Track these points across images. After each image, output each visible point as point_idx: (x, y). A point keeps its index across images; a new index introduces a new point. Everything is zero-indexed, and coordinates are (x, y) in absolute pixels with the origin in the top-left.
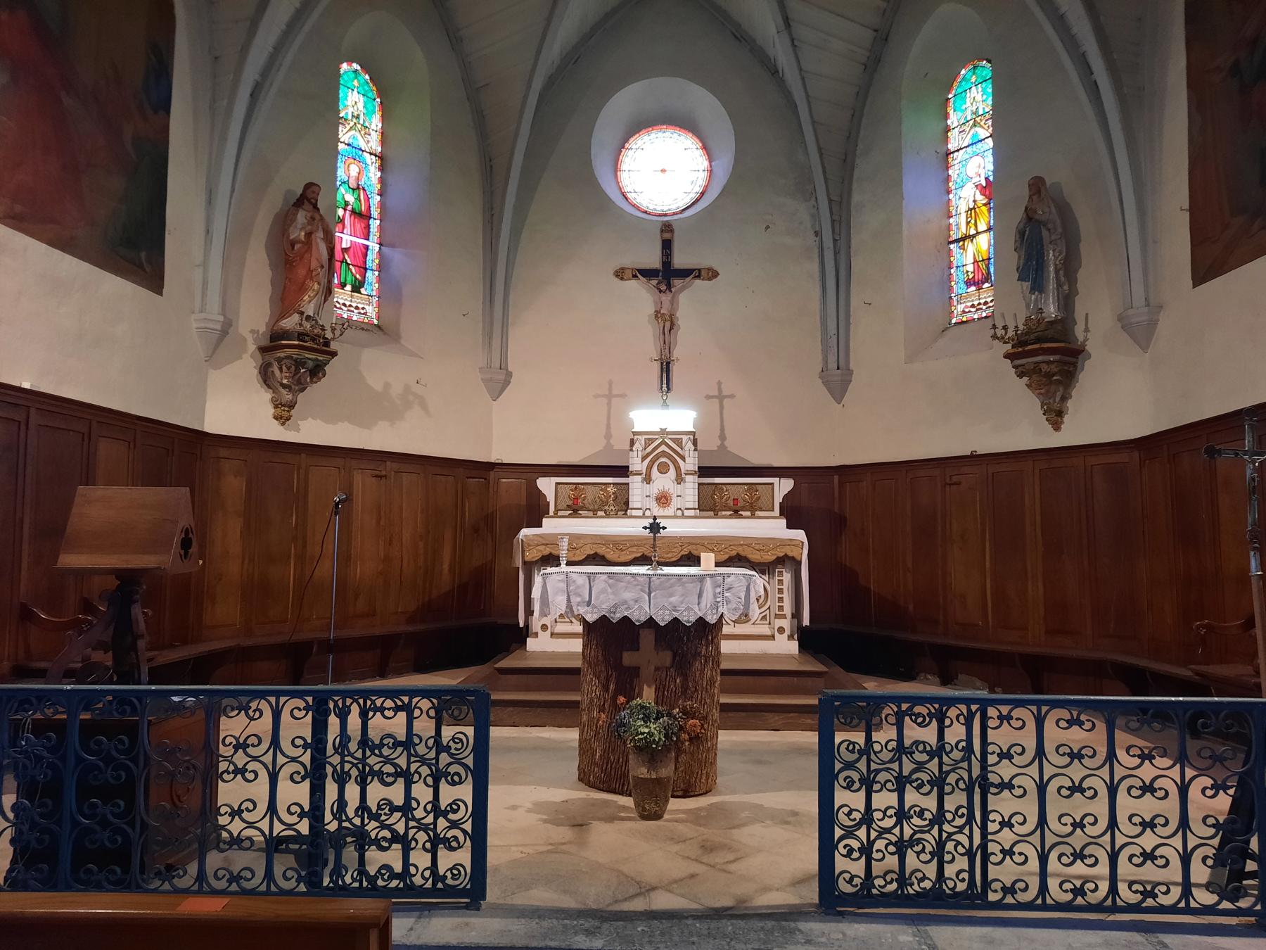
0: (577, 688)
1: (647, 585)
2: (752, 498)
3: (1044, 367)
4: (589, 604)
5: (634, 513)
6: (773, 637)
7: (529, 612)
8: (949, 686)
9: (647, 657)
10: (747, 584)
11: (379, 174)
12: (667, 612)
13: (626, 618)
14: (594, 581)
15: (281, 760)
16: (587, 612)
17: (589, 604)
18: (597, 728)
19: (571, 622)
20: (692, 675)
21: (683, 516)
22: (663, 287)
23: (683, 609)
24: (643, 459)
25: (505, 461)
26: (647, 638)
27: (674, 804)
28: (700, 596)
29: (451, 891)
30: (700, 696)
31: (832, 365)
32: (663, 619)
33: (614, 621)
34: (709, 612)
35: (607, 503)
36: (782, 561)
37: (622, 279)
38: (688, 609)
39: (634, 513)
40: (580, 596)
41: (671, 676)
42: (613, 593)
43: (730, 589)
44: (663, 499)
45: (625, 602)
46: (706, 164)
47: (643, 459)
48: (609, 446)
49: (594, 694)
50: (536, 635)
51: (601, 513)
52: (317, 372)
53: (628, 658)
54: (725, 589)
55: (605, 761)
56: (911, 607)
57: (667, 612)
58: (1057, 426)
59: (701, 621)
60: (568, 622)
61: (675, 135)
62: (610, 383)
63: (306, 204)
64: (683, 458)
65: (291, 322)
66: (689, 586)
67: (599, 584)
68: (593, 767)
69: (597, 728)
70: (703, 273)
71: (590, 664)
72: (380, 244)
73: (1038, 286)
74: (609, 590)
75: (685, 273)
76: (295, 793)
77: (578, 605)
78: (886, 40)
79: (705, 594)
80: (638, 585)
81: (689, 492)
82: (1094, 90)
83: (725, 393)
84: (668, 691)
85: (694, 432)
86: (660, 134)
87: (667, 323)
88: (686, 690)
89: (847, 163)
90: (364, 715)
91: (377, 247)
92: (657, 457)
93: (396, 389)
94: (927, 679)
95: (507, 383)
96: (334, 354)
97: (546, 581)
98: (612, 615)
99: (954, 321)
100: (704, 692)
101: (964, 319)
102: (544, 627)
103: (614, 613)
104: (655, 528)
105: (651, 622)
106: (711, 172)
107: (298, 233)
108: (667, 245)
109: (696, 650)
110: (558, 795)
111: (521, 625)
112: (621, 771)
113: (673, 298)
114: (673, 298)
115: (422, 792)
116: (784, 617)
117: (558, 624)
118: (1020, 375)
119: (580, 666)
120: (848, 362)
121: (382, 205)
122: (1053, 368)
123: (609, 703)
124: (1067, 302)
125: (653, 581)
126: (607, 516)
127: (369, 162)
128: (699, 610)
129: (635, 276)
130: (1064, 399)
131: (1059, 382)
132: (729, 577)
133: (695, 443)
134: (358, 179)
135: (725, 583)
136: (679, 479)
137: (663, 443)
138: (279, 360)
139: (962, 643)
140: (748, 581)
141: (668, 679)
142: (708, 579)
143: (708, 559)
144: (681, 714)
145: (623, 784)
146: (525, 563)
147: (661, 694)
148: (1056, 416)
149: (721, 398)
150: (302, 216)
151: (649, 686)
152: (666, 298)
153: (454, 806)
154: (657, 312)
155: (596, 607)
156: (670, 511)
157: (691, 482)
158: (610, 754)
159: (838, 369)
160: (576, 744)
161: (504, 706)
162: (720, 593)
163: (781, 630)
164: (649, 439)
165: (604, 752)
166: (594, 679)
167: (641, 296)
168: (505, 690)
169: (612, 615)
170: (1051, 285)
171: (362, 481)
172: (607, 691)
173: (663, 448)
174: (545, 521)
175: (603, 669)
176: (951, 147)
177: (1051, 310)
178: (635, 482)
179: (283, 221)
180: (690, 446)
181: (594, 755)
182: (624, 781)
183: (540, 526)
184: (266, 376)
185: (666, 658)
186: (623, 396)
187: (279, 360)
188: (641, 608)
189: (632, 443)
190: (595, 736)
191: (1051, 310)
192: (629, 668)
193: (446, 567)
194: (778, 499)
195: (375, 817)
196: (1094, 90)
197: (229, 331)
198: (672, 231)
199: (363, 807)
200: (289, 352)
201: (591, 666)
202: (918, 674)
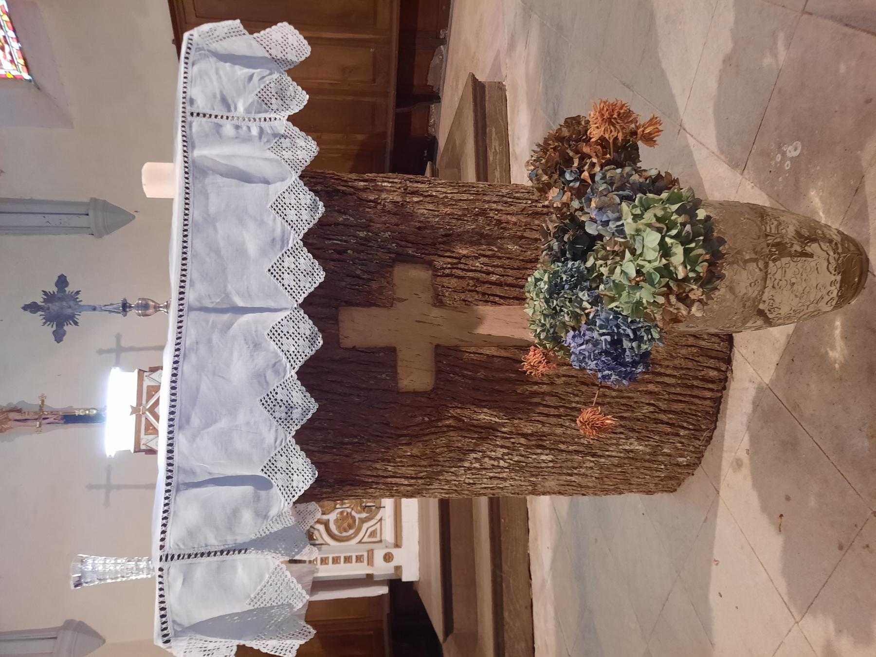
0: (468, 506)
1: (212, 317)
4: (261, 484)
7: (369, 580)
8: (440, 95)
10: (213, 60)
12: (288, 262)
13: (303, 374)
14: (193, 473)
16: (287, 489)
17: (261, 484)
18: (577, 452)
19: (381, 520)
20: (449, 223)
23: (279, 219)
28: (245, 178)
30: (494, 206)
31: (83, 221)
33: (314, 407)
34: (287, 155)
38: (279, 207)
40: (234, 515)
41: (454, 266)
42: (232, 411)
43: (224, 101)
45: (259, 377)
49: (502, 463)
50: (398, 569)
54: (225, 114)
55: (652, 426)
56: (360, 137)
57: (288, 262)
60: (381, 525)
62: (91, 487)
66: (215, 203)
68: (661, 458)
69: (577, 452)
71: (432, 478)
74: (223, 423)
77: (266, 517)
79: (240, 164)
80: (209, 341)
83: (113, 344)
84: (488, 273)
85: (140, 370)
88: (482, 235)
94: (434, 125)
97: (186, 622)
98: (296, 413)
99: (27, 77)
100: (487, 198)
101: (22, 61)
102: (388, 558)
103: (290, 408)
109: (389, 212)
111: (384, 590)
112: (673, 386)
117: (383, 538)
119: (437, 500)
123: (522, 424)
125: (199, 299)
128: (283, 180)
132: (192, 102)
135: (208, 111)
139: (393, 73)
140: (206, 56)
141: (462, 273)
142: (197, 153)
144: (568, 177)
145: (704, 379)
147: (497, 290)
151: (480, 320)
155: (272, 462)
158: (638, 415)
159: (88, 215)
160: (564, 501)
161: (503, 626)
162: (237, 127)
164: (147, 429)
165: (633, 430)
166: (467, 464)
168: (475, 619)
169: (296, 413)
172: (492, 429)
175: (443, 441)
181: (632, 457)
182: (696, 378)
188: (276, 334)
190: (594, 455)
192: (439, 372)
197: (636, 247)
201: (440, 473)
202: (430, 135)
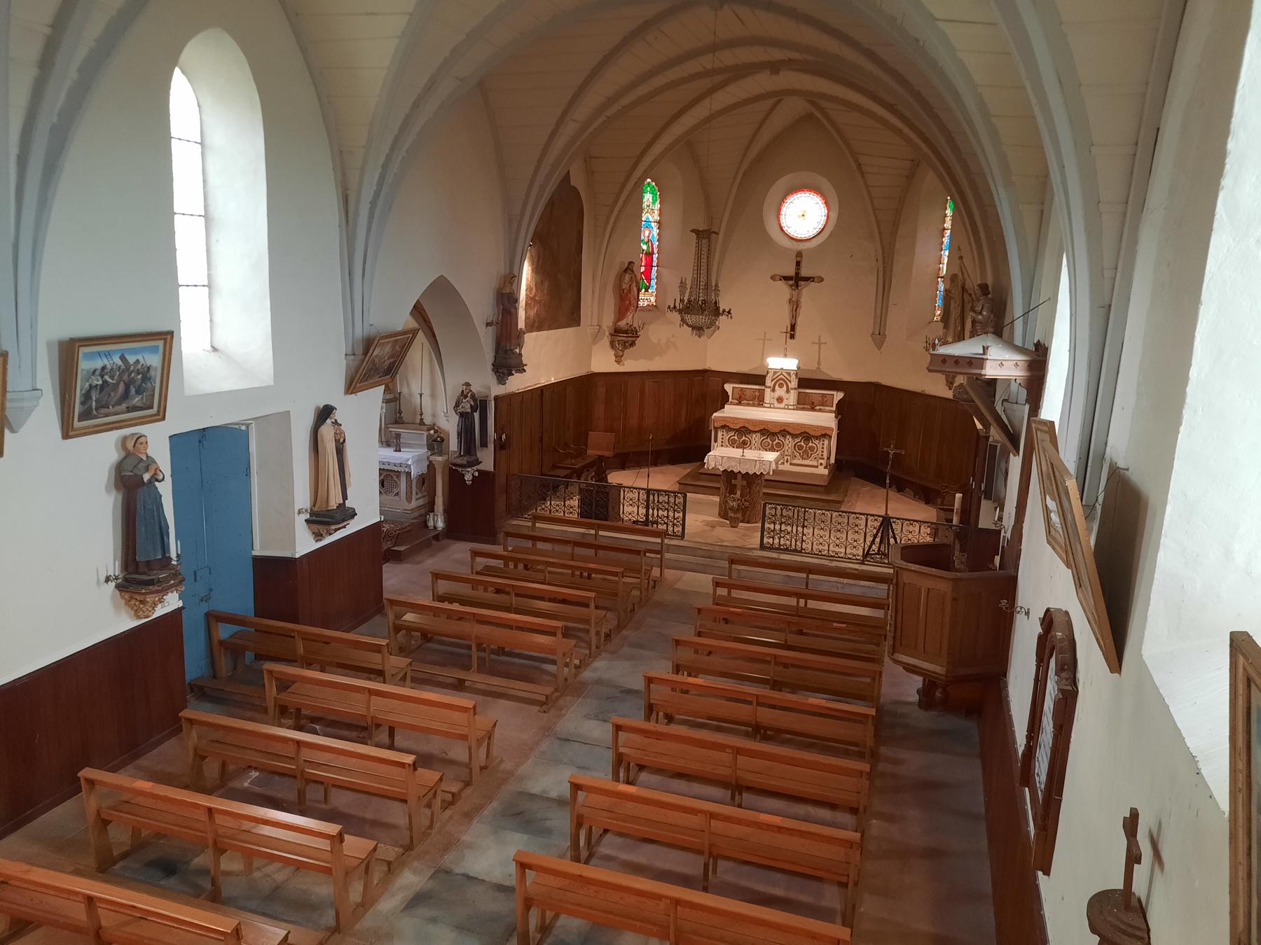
2: (823, 399)
5: (766, 405)
6: (817, 467)
11: (658, 231)
13: (732, 471)
15: (848, 543)
21: (788, 409)
25: (712, 369)
26: (739, 477)
27: (741, 524)
29: (677, 536)
36: (824, 436)
39: (766, 405)
46: (826, 212)
52: (633, 344)
53: (733, 482)
61: (811, 195)
63: (629, 271)
64: (790, 382)
65: (622, 324)
70: (815, 279)
75: (807, 279)
76: (642, 511)
78: (918, 165)
81: (792, 398)
86: (803, 195)
87: (795, 306)
90: (658, 495)
106: (828, 217)
107: (625, 286)
108: (798, 264)
110: (712, 519)
113: (799, 293)
114: (799, 293)
115: (671, 514)
116: (823, 459)
120: (885, 330)
127: (653, 226)
129: (781, 280)
134: (649, 237)
136: (788, 391)
137: (781, 374)
138: (618, 341)
146: (714, 428)
149: (820, 344)
150: (627, 277)
152: (795, 293)
153: (678, 518)
154: (790, 299)
159: (879, 334)
163: (821, 464)
167: (784, 289)
173: (782, 376)
179: (620, 278)
180: (794, 376)
184: (612, 345)
185: (745, 483)
186: (771, 340)
193: (683, 419)
194: (835, 402)
195: (660, 518)
198: (801, 256)
199: (658, 516)
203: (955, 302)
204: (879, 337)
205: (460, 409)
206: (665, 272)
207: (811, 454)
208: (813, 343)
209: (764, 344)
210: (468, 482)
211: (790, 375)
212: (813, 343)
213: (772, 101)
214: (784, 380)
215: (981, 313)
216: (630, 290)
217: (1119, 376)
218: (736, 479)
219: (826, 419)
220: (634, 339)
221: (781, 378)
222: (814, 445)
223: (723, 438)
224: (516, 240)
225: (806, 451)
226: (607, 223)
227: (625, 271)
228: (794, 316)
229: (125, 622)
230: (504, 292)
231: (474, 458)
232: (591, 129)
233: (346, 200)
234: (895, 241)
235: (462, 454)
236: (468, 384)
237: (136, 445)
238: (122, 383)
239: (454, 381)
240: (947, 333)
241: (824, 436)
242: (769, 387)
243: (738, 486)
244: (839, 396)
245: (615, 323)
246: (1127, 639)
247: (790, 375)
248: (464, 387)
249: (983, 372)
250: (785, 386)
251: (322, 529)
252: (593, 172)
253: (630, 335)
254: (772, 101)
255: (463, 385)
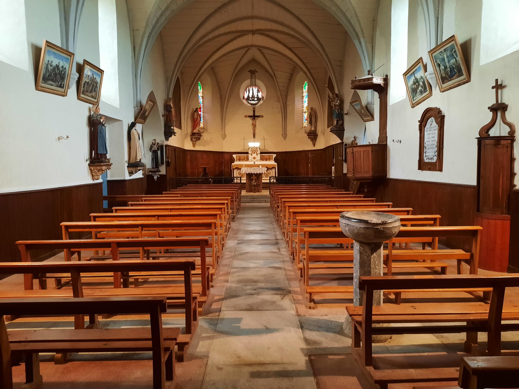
2: (269, 157)
3: (312, 138)
5: (250, 160)
9: (254, 177)
21: (258, 161)
22: (253, 119)
24: (251, 151)
26: (254, 175)
32: (255, 173)
35: (245, 159)
36: (273, 168)
37: (246, 117)
39: (250, 160)
44: (254, 158)
47: (251, 151)
48: (244, 148)
51: (244, 161)
52: (199, 139)
53: (252, 178)
58: (314, 146)
59: (260, 173)
62: (244, 137)
63: (196, 112)
64: (257, 151)
67: (248, 169)
72: (203, 113)
73: (311, 125)
75: (257, 116)
81: (258, 157)
82: (318, 98)
87: (254, 126)
89: (286, 96)
91: (202, 113)
92: (253, 151)
93: (208, 140)
95: (226, 137)
96: (202, 136)
104: (254, 163)
105: (254, 173)
107: (196, 117)
108: (254, 111)
118: (309, 138)
121: (203, 106)
122: (313, 138)
124: (316, 127)
126: (245, 161)
129: (248, 117)
130: (315, 142)
131: (314, 140)
133: (259, 148)
136: (257, 155)
138: (194, 138)
143: (261, 167)
148: (314, 145)
149: (264, 139)
152: (254, 121)
154: (252, 124)
156: (255, 160)
157: (259, 155)
167: (250, 121)
170: (313, 125)
171: (204, 155)
173: (254, 149)
174: (235, 162)
176: (304, 95)
177: (313, 129)
178: (250, 155)
183: (234, 163)
184: (192, 140)
186: (246, 139)
187: (194, 138)
189: (249, 149)
191: (313, 129)
194: (274, 158)
196: (318, 98)
200: (196, 136)
203: (313, 116)
204: (285, 136)
205: (153, 149)
206: (206, 115)
207: (269, 175)
208: (262, 139)
209: (244, 141)
210: (155, 180)
211: (257, 149)
212: (262, 139)
213: (246, 49)
214: (255, 151)
215: (337, 102)
216: (197, 118)
217: (443, 34)
218: (253, 176)
219: (272, 163)
220: (200, 137)
221: (254, 150)
222: (269, 172)
223: (236, 173)
224: (170, 86)
225: (267, 175)
226: (188, 94)
227: (195, 111)
228: (254, 130)
229: (89, 181)
230: (168, 104)
231: (158, 169)
232: (199, 44)
233: (134, 48)
234: (287, 101)
235: (154, 167)
236: (155, 140)
237: (97, 109)
238: (92, 85)
239: (149, 140)
240: (311, 127)
241: (273, 168)
242: (250, 154)
243: (253, 179)
244: (274, 156)
245: (192, 132)
246: (471, 73)
247: (257, 149)
248: (154, 141)
249: (373, 81)
250: (256, 153)
251: (133, 170)
252: (183, 73)
253: (199, 135)
254: (246, 49)
255: (153, 140)
